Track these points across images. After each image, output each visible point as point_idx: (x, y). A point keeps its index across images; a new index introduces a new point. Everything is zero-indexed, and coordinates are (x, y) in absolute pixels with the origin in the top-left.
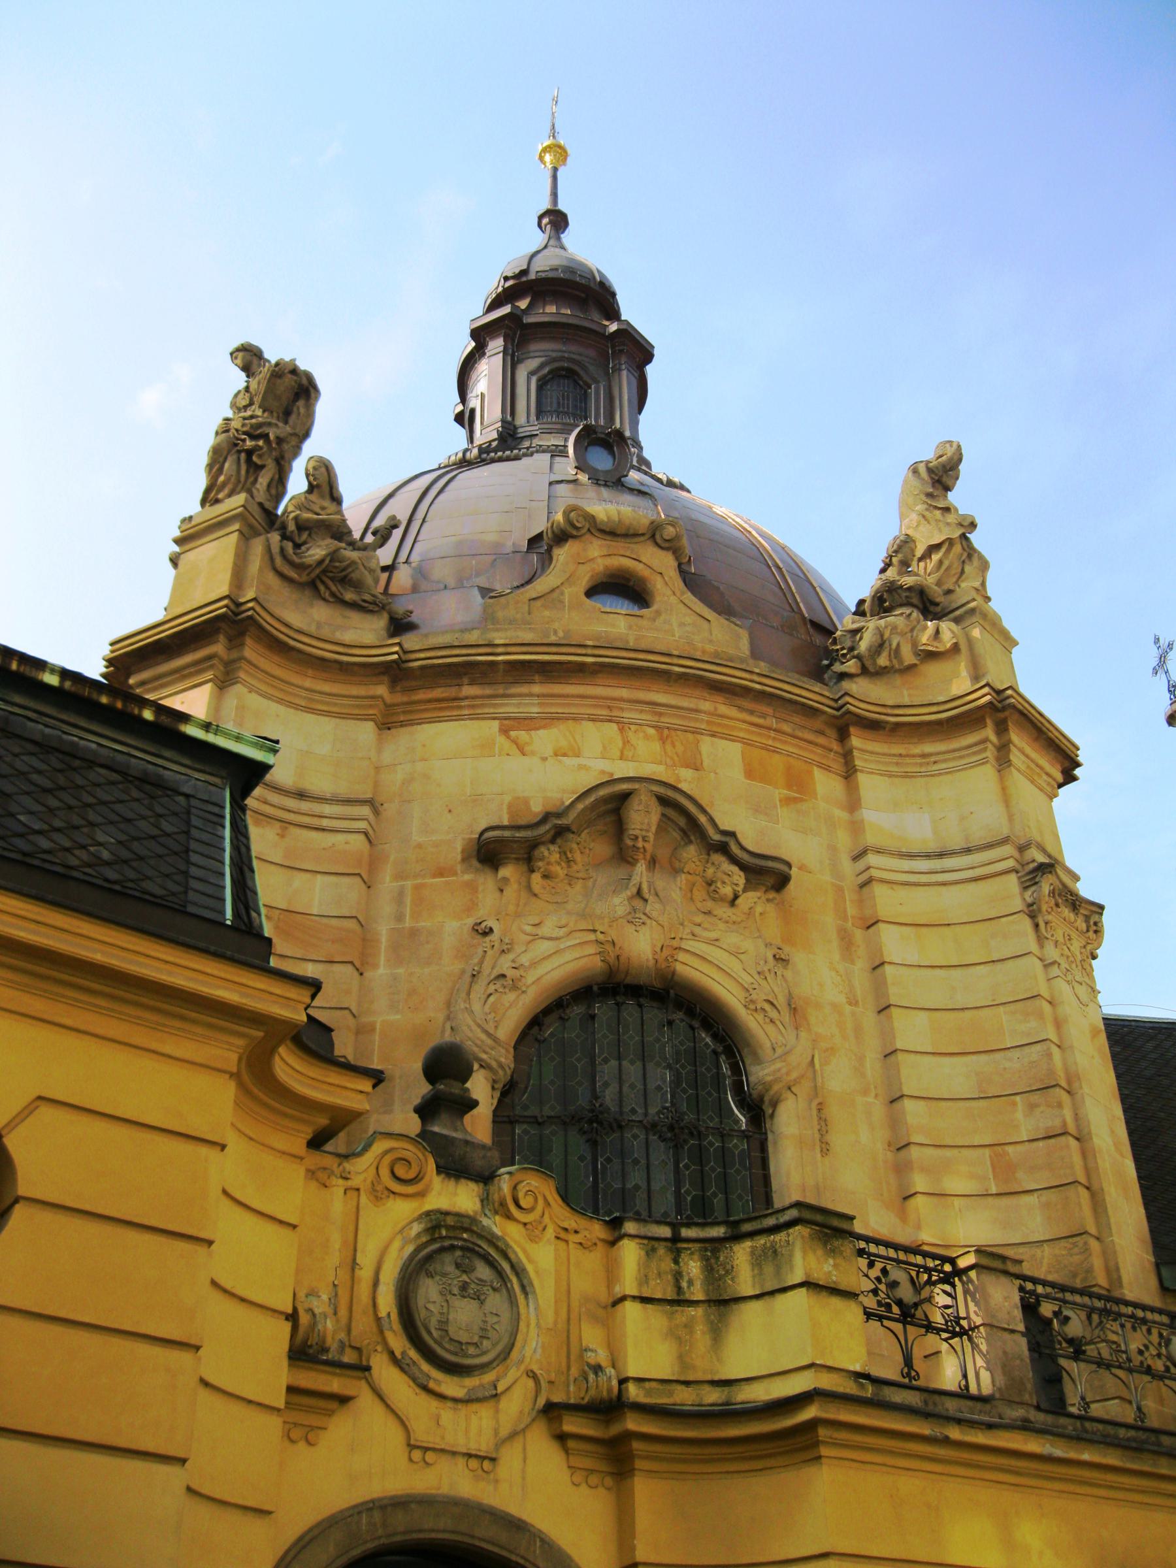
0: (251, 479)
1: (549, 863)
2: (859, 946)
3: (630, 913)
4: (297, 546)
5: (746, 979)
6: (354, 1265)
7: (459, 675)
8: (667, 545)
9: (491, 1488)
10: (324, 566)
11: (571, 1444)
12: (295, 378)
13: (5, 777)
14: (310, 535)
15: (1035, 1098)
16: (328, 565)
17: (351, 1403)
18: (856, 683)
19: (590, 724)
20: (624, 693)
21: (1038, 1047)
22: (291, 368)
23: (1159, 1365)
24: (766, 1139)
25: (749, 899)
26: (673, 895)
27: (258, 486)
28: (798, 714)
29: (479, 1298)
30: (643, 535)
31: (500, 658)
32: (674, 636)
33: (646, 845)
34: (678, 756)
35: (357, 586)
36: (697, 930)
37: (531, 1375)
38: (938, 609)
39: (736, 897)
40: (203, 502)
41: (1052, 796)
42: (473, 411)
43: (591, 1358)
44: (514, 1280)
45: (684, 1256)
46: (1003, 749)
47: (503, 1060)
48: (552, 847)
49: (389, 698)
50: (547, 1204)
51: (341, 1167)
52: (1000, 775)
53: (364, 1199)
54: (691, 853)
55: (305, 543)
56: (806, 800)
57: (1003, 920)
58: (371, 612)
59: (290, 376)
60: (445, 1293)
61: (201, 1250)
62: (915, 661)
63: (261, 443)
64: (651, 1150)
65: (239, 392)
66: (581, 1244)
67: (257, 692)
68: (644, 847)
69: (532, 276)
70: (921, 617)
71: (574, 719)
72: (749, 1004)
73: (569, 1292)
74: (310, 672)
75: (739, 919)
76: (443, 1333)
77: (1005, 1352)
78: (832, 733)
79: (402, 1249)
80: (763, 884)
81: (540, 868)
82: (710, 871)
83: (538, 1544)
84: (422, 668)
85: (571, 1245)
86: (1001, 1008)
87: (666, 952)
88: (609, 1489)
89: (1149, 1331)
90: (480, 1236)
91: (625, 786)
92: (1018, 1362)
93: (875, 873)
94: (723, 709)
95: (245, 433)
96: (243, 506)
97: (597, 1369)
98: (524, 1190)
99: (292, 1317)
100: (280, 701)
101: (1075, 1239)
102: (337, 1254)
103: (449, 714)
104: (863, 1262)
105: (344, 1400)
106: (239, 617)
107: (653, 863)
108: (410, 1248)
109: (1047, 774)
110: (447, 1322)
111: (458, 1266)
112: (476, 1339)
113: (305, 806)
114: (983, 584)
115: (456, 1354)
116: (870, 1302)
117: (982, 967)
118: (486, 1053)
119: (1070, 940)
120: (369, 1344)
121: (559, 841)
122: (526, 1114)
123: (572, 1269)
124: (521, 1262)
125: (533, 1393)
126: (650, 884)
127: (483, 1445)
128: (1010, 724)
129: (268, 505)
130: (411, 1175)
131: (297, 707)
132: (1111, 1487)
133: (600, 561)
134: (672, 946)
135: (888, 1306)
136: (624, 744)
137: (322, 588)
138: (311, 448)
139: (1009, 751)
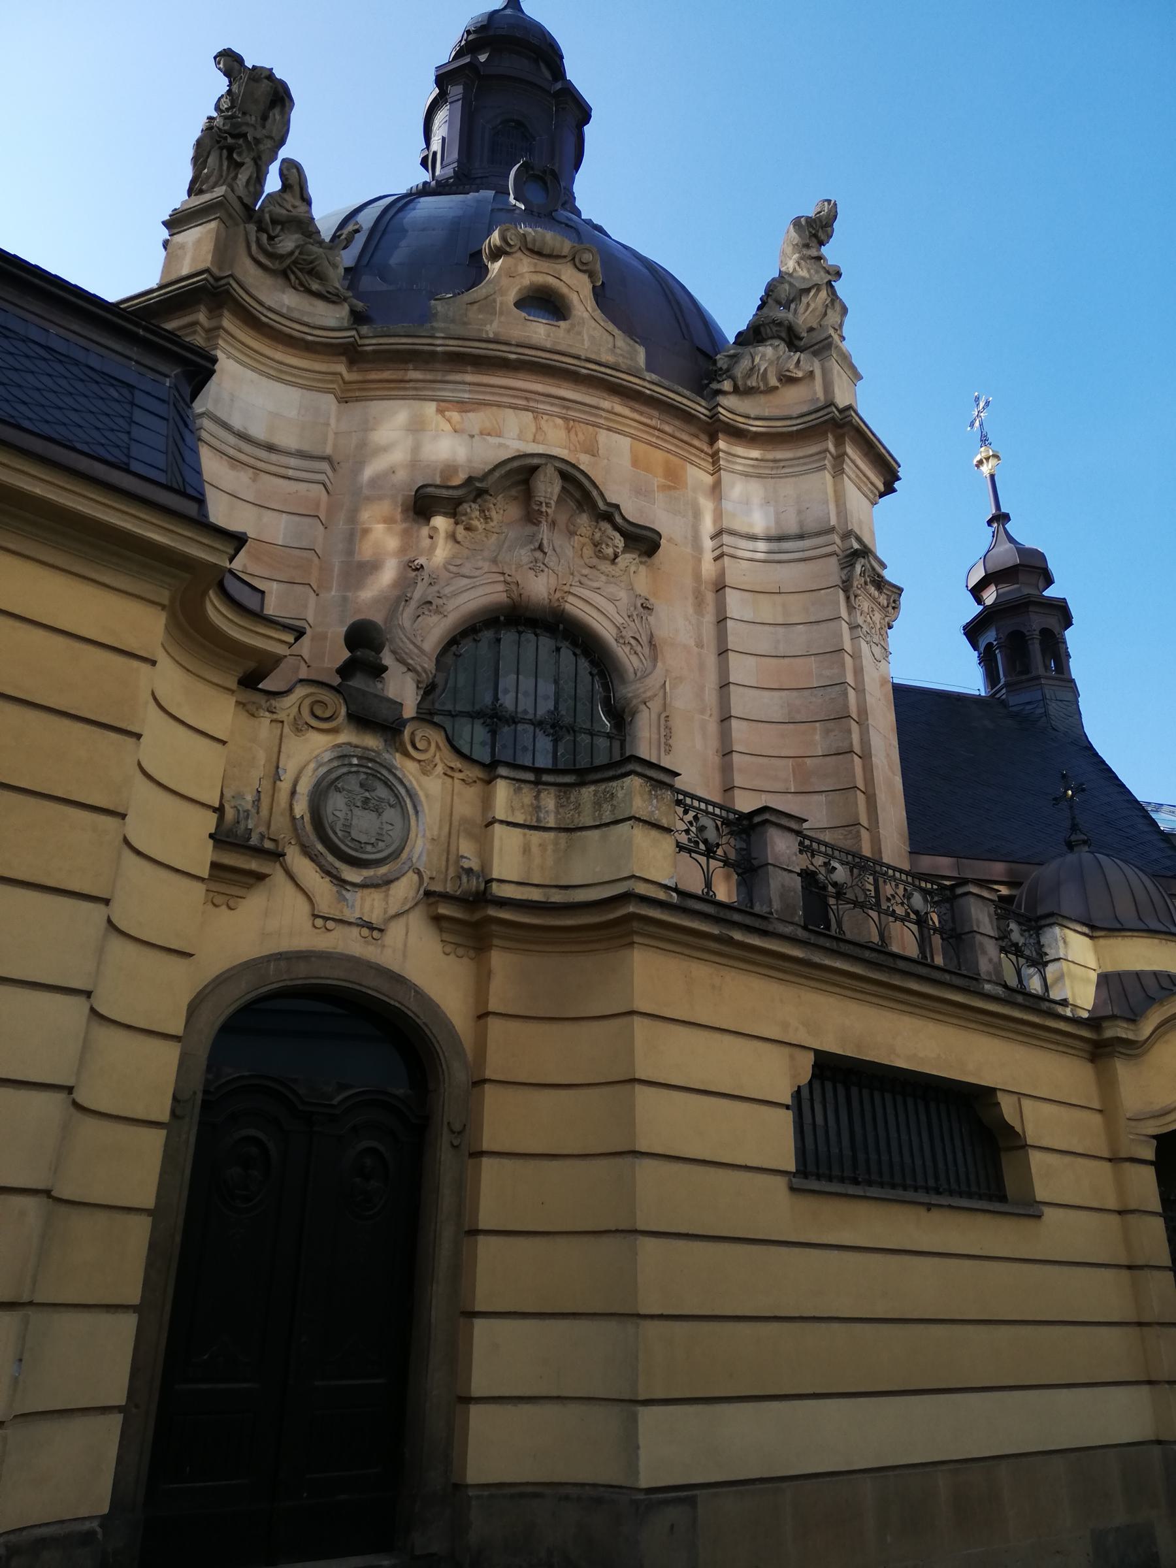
0: (232, 175)
1: (471, 519)
2: (708, 605)
3: (532, 562)
4: (271, 238)
5: (619, 620)
6: (277, 777)
7: (406, 361)
8: (584, 268)
9: (379, 951)
10: (293, 258)
11: (445, 924)
12: (271, 84)
13: (4, 384)
14: (282, 230)
15: (830, 725)
16: (297, 258)
17: (267, 879)
18: (728, 399)
19: (511, 411)
20: (539, 387)
21: (837, 688)
22: (267, 73)
23: (900, 911)
24: (625, 740)
25: (626, 559)
26: (567, 551)
27: (238, 182)
28: (679, 418)
29: (378, 811)
30: (565, 257)
31: (439, 349)
32: (583, 344)
33: (549, 511)
34: (579, 444)
35: (321, 277)
36: (584, 580)
37: (416, 871)
38: (802, 343)
39: (616, 556)
40: (190, 192)
41: (874, 503)
42: (435, 154)
43: (466, 864)
44: (408, 801)
45: (542, 795)
46: (840, 458)
47: (426, 666)
48: (473, 505)
49: (348, 376)
50: (438, 746)
51: (268, 703)
52: (834, 482)
53: (287, 730)
54: (584, 520)
55: (277, 236)
56: (678, 489)
57: (823, 591)
58: (334, 302)
59: (266, 81)
60: (351, 804)
61: (130, 741)
62: (778, 384)
63: (241, 141)
64: (537, 740)
65: (222, 96)
66: (463, 780)
67: (233, 359)
68: (546, 512)
69: (491, 33)
70: (787, 349)
71: (499, 406)
72: (620, 638)
73: (451, 814)
74: (280, 347)
75: (617, 574)
76: (346, 834)
77: (783, 886)
78: (705, 437)
79: (316, 769)
80: (638, 550)
81: (463, 522)
82: (598, 536)
83: (413, 993)
84: (375, 352)
85: (456, 781)
86: (813, 658)
87: (558, 595)
88: (472, 959)
89: (897, 886)
90: (381, 765)
91: (536, 461)
92: (792, 893)
93: (725, 549)
94: (619, 408)
95: (226, 132)
96: (223, 196)
97: (469, 871)
98: (421, 735)
99: (220, 810)
100: (254, 369)
101: (852, 828)
102: (262, 768)
103: (396, 393)
104: (680, 810)
105: (261, 877)
106: (218, 290)
107: (553, 524)
108: (323, 770)
109: (872, 483)
110: (350, 826)
111: (362, 785)
112: (373, 840)
113: (274, 457)
114: (841, 325)
115: (356, 850)
116: (683, 838)
117: (801, 626)
118: (413, 659)
119: (873, 611)
120: (284, 837)
121: (479, 500)
122: (443, 708)
123: (455, 797)
124: (415, 789)
125: (418, 884)
126: (550, 541)
127: (375, 918)
128: (847, 439)
129: (247, 200)
130: (327, 715)
131: (269, 376)
132: (856, 990)
133: (527, 275)
134: (562, 590)
135: (697, 843)
136: (537, 429)
137: (292, 277)
138: (283, 153)
139: (843, 461)
